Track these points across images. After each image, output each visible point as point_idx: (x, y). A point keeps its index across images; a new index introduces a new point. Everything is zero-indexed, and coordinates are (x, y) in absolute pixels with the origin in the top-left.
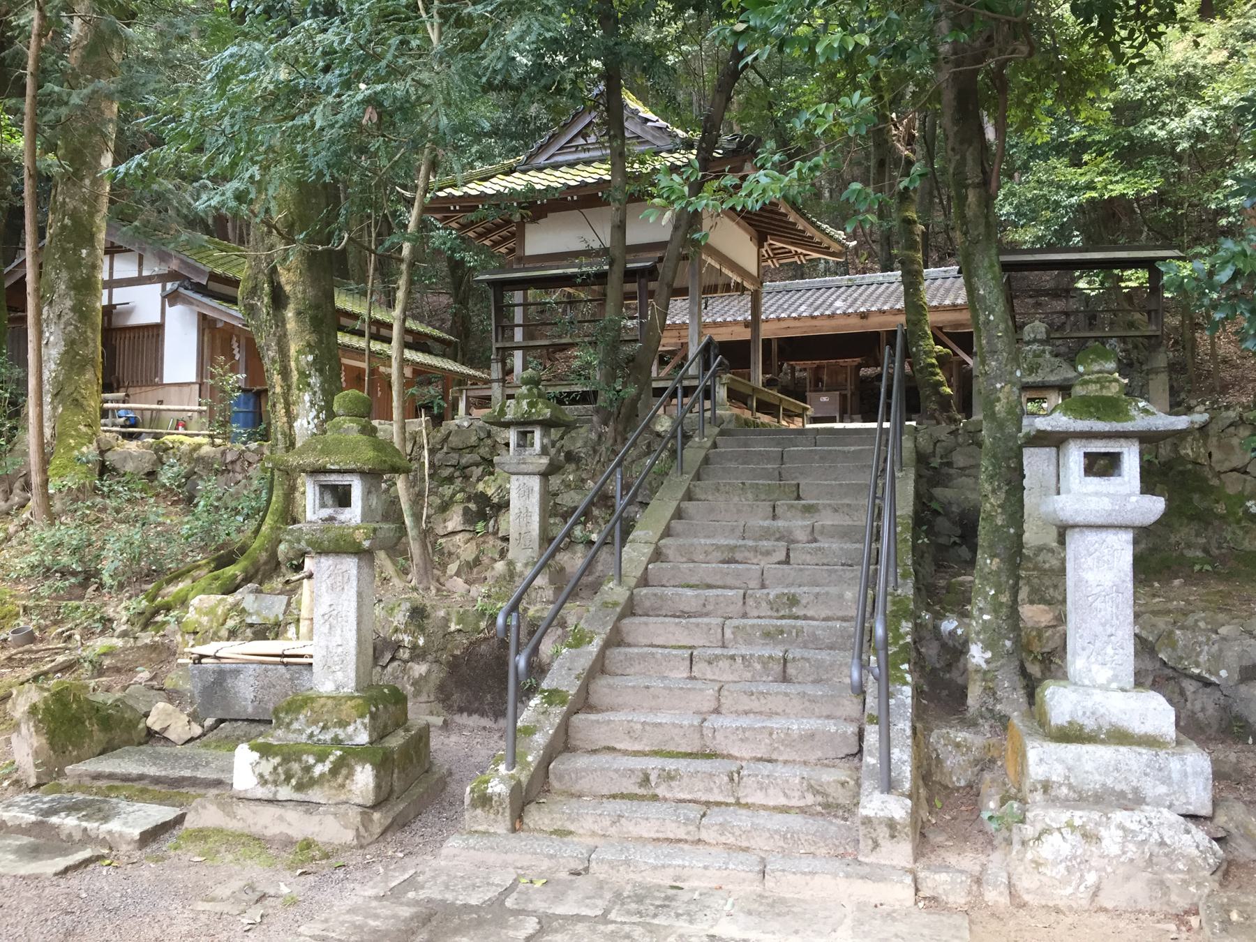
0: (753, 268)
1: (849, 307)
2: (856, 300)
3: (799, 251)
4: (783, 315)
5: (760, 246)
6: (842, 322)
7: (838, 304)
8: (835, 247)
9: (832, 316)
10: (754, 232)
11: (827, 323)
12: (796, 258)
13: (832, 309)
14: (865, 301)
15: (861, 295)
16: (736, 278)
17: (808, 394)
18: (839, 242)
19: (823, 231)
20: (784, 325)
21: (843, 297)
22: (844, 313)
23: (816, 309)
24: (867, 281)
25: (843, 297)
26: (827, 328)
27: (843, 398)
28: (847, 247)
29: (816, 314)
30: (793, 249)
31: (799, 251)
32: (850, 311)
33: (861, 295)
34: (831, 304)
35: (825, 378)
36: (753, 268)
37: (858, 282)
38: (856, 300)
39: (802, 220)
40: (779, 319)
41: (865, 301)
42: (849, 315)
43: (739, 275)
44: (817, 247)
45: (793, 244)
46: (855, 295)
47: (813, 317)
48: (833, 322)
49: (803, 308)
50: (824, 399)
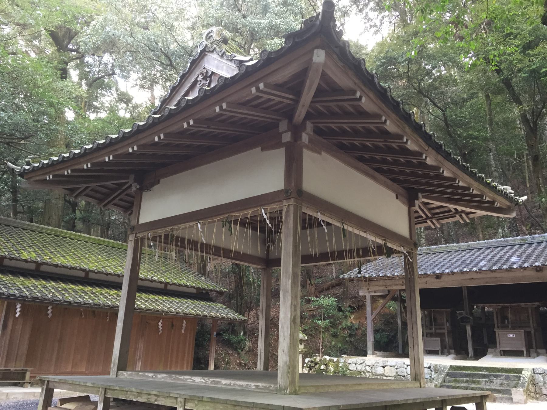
0: (403, 229)
1: (525, 262)
2: (529, 256)
3: (460, 208)
4: (465, 269)
5: (411, 204)
6: (521, 274)
7: (514, 259)
8: (500, 202)
9: (510, 269)
10: (401, 190)
11: (506, 275)
12: (458, 218)
13: (509, 264)
14: (539, 256)
15: (534, 251)
16: (372, 238)
17: (496, 330)
18: (505, 195)
19: (494, 189)
20: (467, 276)
21: (518, 253)
22: (521, 267)
23: (494, 264)
24: (536, 240)
25: (518, 253)
26: (507, 280)
27: (528, 334)
28: (517, 203)
29: (494, 268)
30: (452, 206)
31: (460, 208)
32: (526, 265)
33: (534, 251)
34: (508, 260)
35: (510, 316)
36: (403, 229)
37: (529, 241)
38: (529, 256)
39: (475, 184)
40: (462, 272)
41: (539, 256)
42: (525, 269)
43: (378, 235)
44: (490, 206)
45: (450, 201)
46: (529, 251)
47: (491, 271)
48: (511, 274)
49: (483, 263)
50: (511, 335)
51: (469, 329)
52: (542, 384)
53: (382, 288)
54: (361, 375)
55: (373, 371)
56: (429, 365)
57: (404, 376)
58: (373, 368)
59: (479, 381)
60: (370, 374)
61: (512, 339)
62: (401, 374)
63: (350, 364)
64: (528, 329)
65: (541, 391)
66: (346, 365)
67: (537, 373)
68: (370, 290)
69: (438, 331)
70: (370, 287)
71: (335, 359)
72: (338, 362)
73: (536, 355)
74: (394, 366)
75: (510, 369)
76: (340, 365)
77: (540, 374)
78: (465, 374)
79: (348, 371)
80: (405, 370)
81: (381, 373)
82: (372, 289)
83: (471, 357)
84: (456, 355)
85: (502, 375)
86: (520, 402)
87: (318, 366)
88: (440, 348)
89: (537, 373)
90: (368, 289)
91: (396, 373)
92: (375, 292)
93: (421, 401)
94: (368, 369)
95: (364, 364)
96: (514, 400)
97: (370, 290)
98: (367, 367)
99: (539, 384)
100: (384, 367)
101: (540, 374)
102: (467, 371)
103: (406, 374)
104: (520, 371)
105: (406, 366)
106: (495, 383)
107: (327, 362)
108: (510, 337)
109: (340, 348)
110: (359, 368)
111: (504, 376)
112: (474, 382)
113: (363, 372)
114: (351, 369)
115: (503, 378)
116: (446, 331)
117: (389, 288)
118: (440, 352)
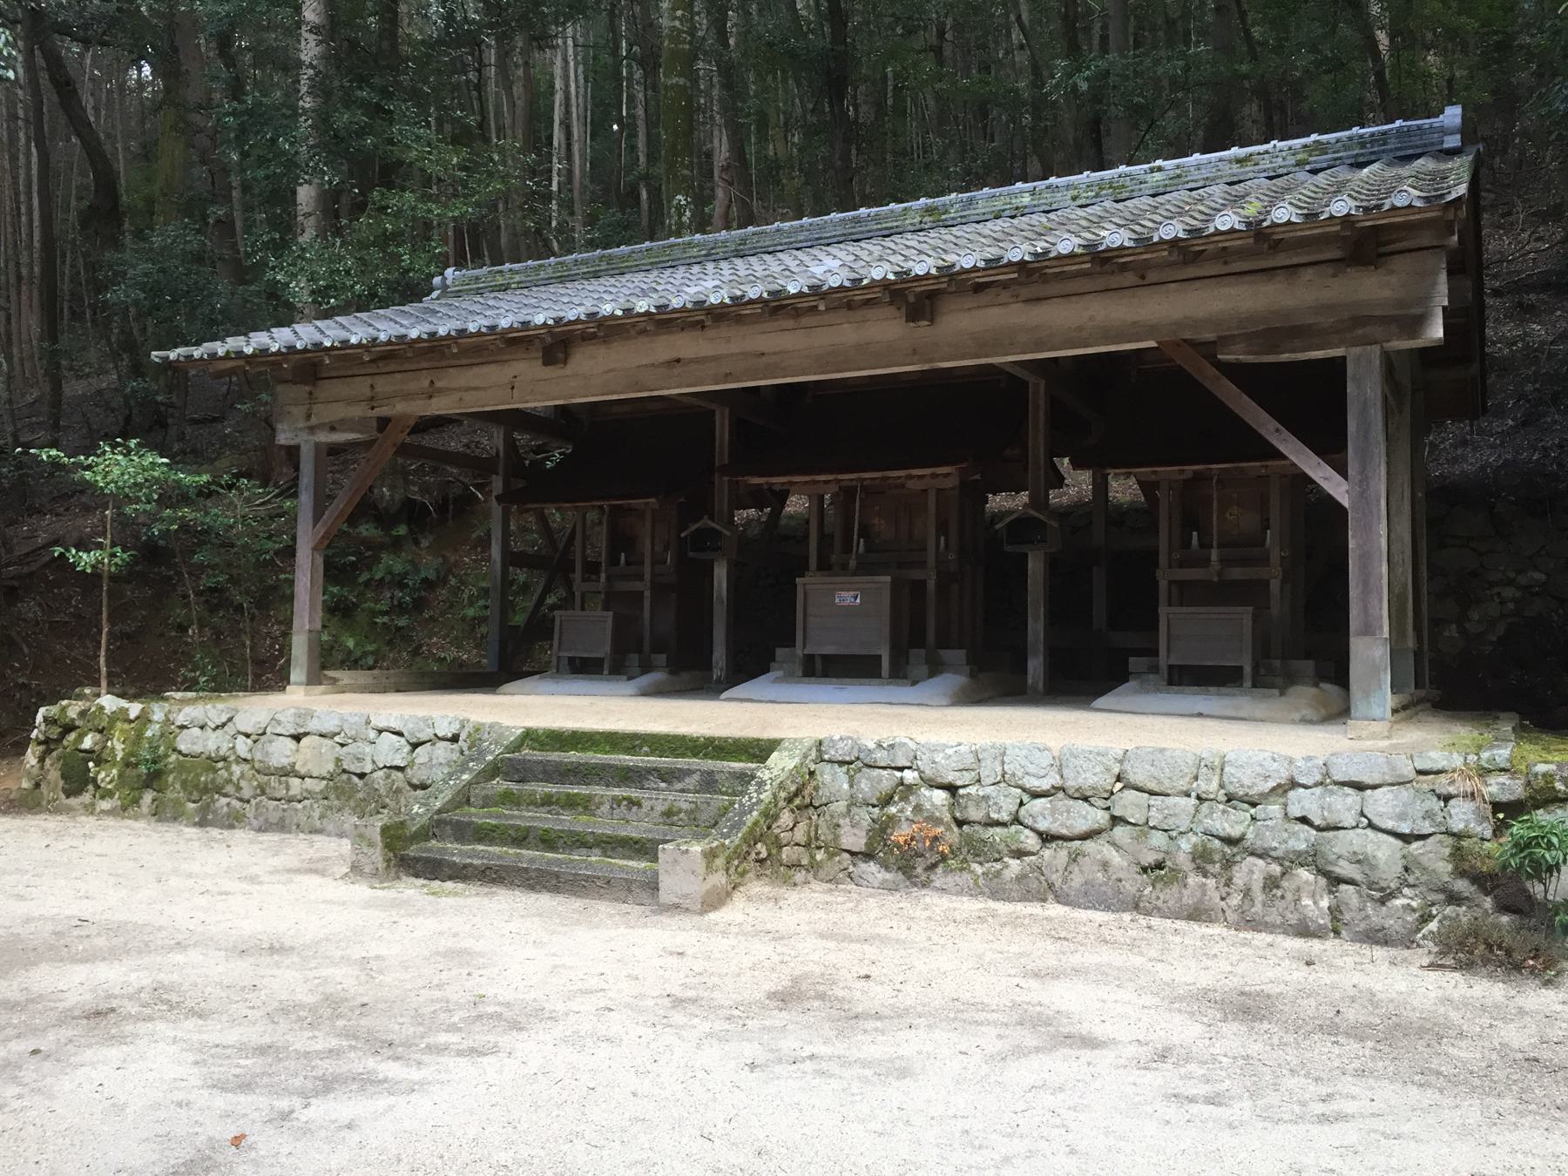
50: (847, 598)
51: (721, 574)
52: (841, 806)
53: (358, 411)
54: (216, 771)
55: (258, 756)
56: (454, 729)
57: (362, 776)
58: (259, 745)
59: (589, 798)
60: (246, 767)
61: (848, 611)
62: (352, 769)
63: (183, 727)
64: (916, 574)
65: (836, 837)
66: (170, 731)
67: (830, 761)
68: (314, 421)
69: (1237, 573)
70: (316, 408)
71: (135, 709)
72: (144, 719)
73: (924, 669)
74: (333, 735)
75: (737, 741)
76: (149, 734)
77: (842, 763)
78: (558, 764)
79: (173, 757)
80: (368, 749)
81: (285, 761)
82: (324, 413)
83: (719, 681)
84: (672, 673)
85: (689, 772)
86: (686, 903)
87: (72, 736)
88: (608, 649)
89: (830, 761)
90: (309, 416)
91: (338, 760)
92: (333, 429)
93: (413, 879)
94: (242, 746)
95: (230, 729)
96: (665, 896)
97: (314, 421)
98: (241, 738)
99: (832, 807)
100: (297, 738)
101: (842, 763)
102: (584, 750)
103: (368, 768)
104: (760, 750)
105: (372, 735)
106: (646, 805)
107: (104, 724)
108: (845, 603)
109: (350, 652)
110: (212, 743)
111: (696, 777)
112: (571, 803)
113: (225, 759)
114: (182, 747)
115: (692, 781)
116: (644, 587)
117: (383, 411)
118: (606, 666)
